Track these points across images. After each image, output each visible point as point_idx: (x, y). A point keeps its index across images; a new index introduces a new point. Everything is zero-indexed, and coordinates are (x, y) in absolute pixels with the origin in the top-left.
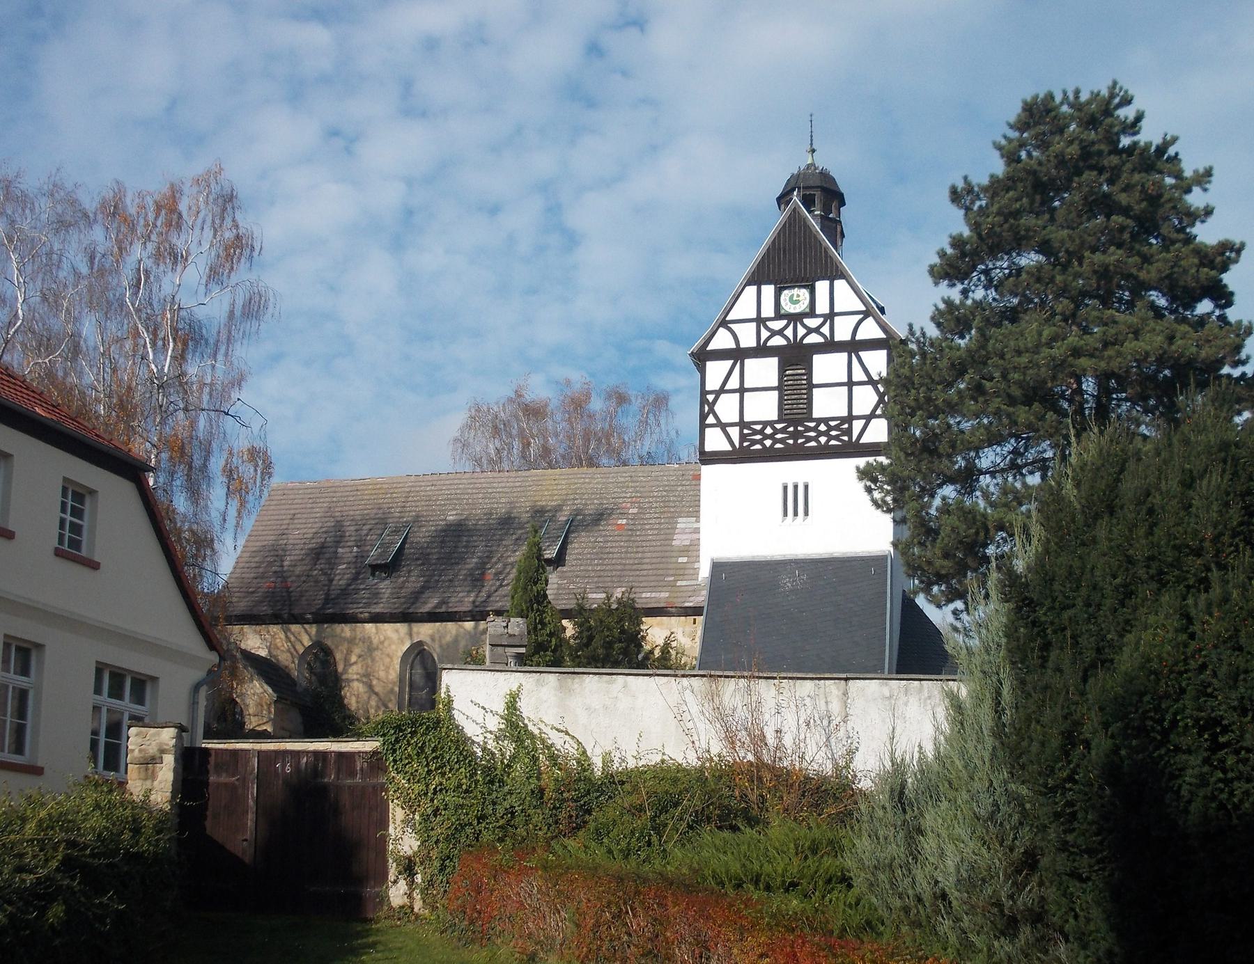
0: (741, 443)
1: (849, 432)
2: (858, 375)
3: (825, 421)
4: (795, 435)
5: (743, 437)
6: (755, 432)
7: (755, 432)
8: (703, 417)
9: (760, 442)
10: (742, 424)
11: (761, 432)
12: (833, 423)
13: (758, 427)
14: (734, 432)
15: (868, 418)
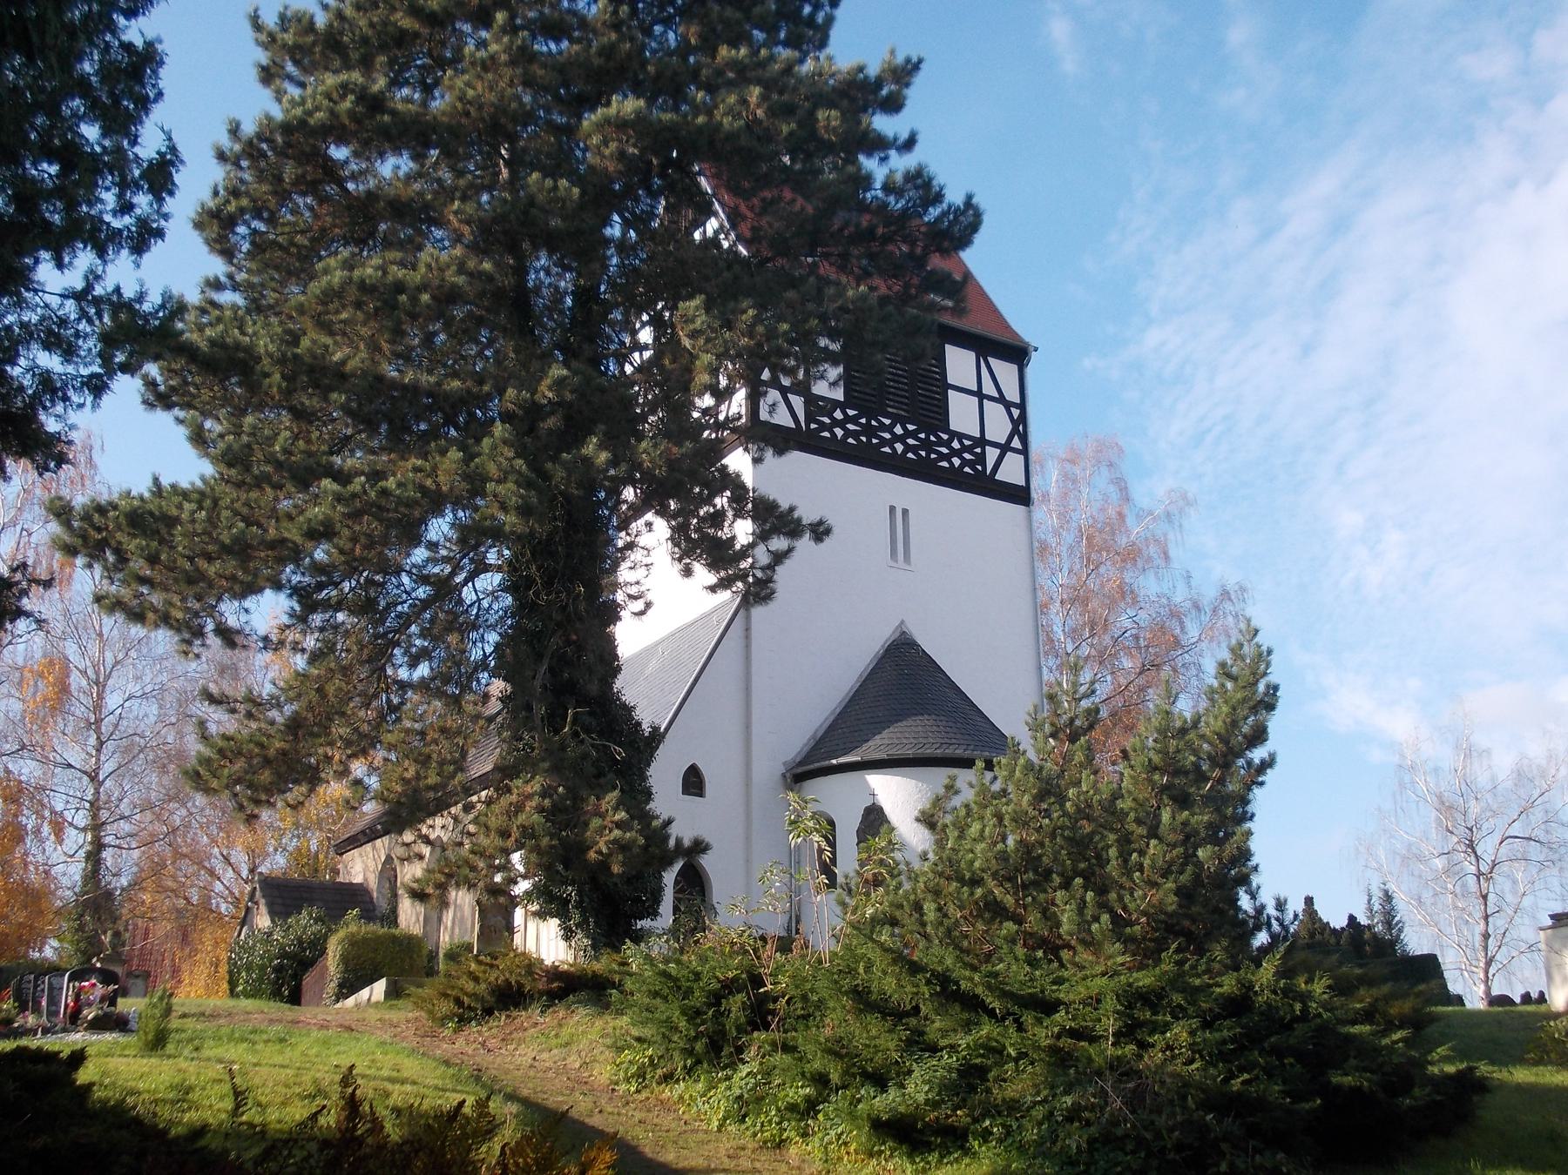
0: (809, 419)
1: (981, 459)
2: (989, 388)
3: (961, 436)
4: (926, 445)
8: (1023, 418)
12: (967, 443)
15: (1005, 448)
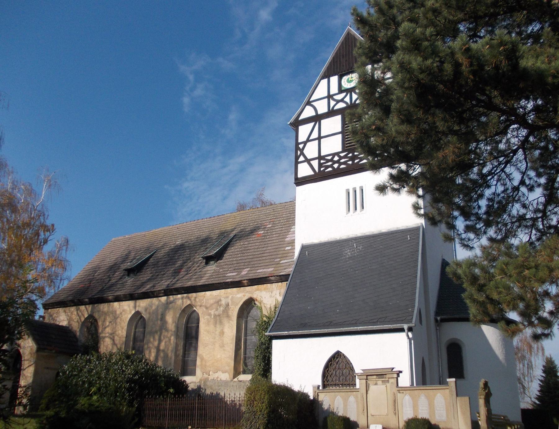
5: (320, 165)
6: (328, 161)
7: (328, 161)
9: (331, 166)
10: (320, 158)
11: (332, 160)
13: (329, 158)
14: (315, 164)
